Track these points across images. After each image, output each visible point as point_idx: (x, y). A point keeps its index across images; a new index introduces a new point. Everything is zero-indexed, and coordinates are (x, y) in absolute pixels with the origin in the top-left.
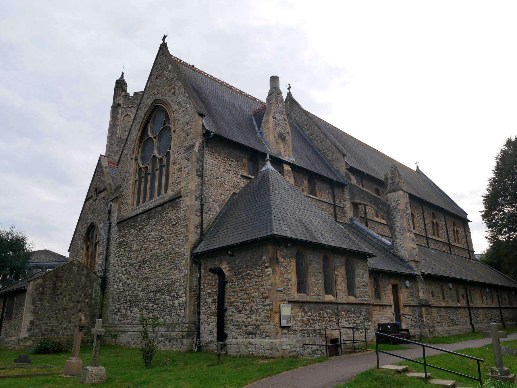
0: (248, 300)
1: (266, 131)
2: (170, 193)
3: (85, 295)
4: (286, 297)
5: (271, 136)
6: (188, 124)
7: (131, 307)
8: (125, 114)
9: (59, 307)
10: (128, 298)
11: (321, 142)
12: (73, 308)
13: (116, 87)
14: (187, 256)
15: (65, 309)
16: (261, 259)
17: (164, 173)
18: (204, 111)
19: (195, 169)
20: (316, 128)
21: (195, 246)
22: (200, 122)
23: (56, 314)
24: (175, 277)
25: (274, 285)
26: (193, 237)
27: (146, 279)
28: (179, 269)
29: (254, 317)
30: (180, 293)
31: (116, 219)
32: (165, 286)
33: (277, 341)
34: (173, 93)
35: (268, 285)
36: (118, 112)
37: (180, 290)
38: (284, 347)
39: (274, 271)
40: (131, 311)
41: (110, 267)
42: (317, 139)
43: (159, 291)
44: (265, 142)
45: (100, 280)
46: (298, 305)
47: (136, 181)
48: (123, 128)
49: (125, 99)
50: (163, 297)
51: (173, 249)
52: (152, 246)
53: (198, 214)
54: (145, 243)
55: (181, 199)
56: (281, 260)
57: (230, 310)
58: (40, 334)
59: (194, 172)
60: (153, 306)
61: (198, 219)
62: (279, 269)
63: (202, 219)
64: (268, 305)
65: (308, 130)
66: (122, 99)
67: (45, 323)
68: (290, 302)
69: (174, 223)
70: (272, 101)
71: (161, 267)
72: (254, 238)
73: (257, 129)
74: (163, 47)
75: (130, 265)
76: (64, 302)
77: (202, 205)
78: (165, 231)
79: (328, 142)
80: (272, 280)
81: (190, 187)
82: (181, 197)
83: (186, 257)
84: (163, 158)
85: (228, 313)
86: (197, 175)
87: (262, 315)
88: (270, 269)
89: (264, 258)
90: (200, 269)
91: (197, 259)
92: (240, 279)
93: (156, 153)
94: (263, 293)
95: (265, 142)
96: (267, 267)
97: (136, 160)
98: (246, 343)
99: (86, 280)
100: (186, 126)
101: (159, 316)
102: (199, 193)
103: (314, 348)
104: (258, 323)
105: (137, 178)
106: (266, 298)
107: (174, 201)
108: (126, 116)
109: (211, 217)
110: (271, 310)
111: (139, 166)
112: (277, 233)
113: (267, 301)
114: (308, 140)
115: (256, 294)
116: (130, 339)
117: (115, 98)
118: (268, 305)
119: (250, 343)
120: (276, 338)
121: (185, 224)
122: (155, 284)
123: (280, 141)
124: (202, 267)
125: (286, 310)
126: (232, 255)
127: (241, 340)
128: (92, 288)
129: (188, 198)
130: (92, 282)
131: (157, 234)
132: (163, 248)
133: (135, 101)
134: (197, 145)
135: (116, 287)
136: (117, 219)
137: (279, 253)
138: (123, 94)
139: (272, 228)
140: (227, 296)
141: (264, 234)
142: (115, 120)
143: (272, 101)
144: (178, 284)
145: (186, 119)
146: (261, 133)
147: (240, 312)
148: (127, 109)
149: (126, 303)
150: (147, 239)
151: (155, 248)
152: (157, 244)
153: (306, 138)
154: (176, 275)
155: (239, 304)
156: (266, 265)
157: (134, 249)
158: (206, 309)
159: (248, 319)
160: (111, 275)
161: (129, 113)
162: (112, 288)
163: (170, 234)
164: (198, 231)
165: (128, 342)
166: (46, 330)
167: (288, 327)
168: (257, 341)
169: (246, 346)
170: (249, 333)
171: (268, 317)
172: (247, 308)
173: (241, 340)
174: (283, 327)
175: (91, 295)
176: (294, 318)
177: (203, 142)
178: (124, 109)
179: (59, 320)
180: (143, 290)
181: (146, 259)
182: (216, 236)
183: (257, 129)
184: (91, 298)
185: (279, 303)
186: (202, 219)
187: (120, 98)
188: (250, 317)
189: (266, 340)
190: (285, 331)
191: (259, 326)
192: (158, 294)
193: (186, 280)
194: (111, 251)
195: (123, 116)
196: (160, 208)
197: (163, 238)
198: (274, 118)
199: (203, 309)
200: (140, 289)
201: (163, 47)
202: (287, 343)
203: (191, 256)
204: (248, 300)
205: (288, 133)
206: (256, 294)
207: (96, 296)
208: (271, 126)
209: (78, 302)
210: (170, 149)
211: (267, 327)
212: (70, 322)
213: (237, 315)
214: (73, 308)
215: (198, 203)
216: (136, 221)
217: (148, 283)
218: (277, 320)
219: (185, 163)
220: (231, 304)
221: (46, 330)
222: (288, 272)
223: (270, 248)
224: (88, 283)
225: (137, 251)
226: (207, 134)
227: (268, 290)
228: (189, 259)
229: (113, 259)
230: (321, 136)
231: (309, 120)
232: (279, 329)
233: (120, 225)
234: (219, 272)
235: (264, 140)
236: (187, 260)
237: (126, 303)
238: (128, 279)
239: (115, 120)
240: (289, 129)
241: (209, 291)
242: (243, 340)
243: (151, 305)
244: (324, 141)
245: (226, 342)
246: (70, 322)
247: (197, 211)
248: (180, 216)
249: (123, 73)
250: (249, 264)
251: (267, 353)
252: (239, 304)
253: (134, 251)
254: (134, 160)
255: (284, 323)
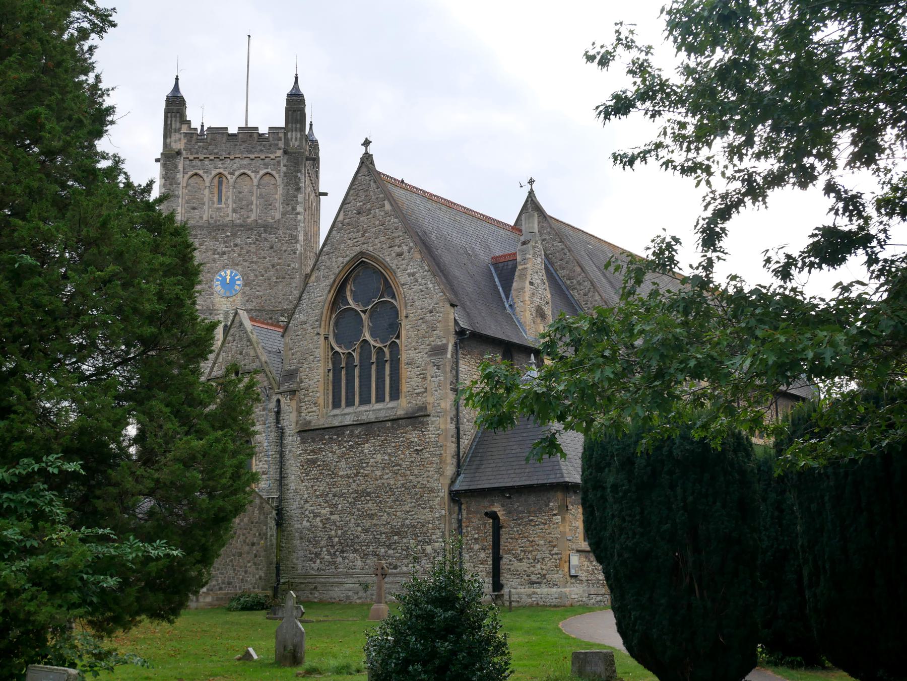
0: (531, 549)
1: (519, 305)
2: (403, 406)
3: (260, 534)
4: (574, 546)
5: (528, 314)
6: (431, 312)
7: (343, 552)
8: (190, 173)
9: (234, 551)
10: (336, 539)
11: (585, 295)
12: (248, 553)
13: (167, 112)
14: (444, 493)
15: (240, 554)
16: (547, 505)
17: (387, 372)
18: (455, 301)
19: (449, 382)
20: (578, 269)
21: (453, 482)
22: (452, 314)
23: (231, 561)
24: (423, 517)
25: (563, 534)
26: (450, 470)
27: (371, 516)
28: (431, 507)
29: (538, 566)
30: (434, 537)
31: (294, 425)
32: (409, 528)
33: (567, 590)
34: (400, 255)
35: (556, 533)
36: (176, 168)
37: (434, 534)
38: (573, 596)
39: (563, 519)
40: (344, 558)
41: (290, 494)
42: (577, 287)
43: (397, 534)
44: (519, 322)
45: (274, 512)
46: (584, 554)
47: (329, 370)
48: (187, 202)
49: (189, 141)
50: (405, 540)
51: (419, 482)
52: (378, 473)
53: (454, 440)
54: (363, 468)
55: (428, 419)
56: (570, 507)
57: (506, 559)
58: (217, 587)
59: (448, 387)
60: (386, 552)
61: (454, 446)
62: (569, 517)
63: (458, 447)
64: (556, 554)
65: (564, 268)
66: (184, 141)
67: (222, 574)
68: (578, 551)
69: (418, 448)
70: (528, 256)
71: (397, 503)
72: (540, 482)
73: (505, 300)
74: (367, 161)
75: (335, 496)
76: (239, 545)
77: (458, 429)
78: (402, 456)
79: (597, 297)
80: (561, 529)
81: (443, 405)
82: (429, 416)
83: (441, 494)
84: (386, 350)
85: (504, 561)
86: (452, 389)
87: (549, 563)
88: (559, 517)
89: (551, 504)
90: (460, 509)
91: (456, 497)
92: (520, 525)
93: (367, 336)
94: (550, 542)
95: (519, 322)
96: (555, 515)
97: (326, 338)
98: (530, 593)
99: (260, 513)
100: (429, 315)
101: (399, 564)
102: (454, 413)
103: (599, 599)
104: (544, 572)
105: (330, 367)
106: (554, 546)
107: (417, 418)
108: (192, 176)
109: (466, 442)
110: (560, 559)
111: (332, 349)
112: (567, 480)
113: (555, 550)
114: (563, 287)
115: (542, 542)
116: (350, 593)
117: (166, 136)
118: (556, 554)
119: (534, 593)
120: (566, 587)
121: (438, 452)
122: (388, 523)
123: (539, 320)
124: (463, 507)
125: (575, 560)
126: (509, 498)
127: (523, 590)
128: (266, 524)
129: (441, 420)
130: (266, 515)
131: (386, 458)
132: (400, 478)
133: (211, 148)
134: (450, 347)
135: (305, 524)
136: (297, 423)
137: (568, 500)
138: (184, 129)
139: (562, 473)
140: (502, 543)
141: (552, 480)
142: (171, 184)
143: (528, 256)
144: (431, 526)
145: (428, 303)
146: (510, 306)
147: (520, 560)
148: (194, 163)
149: (333, 546)
150: (367, 463)
151: (385, 477)
152: (387, 471)
153: (559, 281)
154: (424, 515)
155: (519, 552)
156: (555, 512)
157: (341, 473)
158: (470, 556)
159: (532, 569)
160: (293, 507)
161: (201, 172)
162: (298, 524)
163: (412, 462)
164: (455, 461)
165: (348, 597)
166: (223, 583)
167: (576, 576)
168: (543, 590)
169: (529, 596)
170: (532, 583)
171: (556, 566)
172: (530, 556)
173: (523, 590)
174: (572, 577)
175: (266, 534)
176: (580, 567)
177: (456, 343)
178: (188, 162)
179: (235, 570)
180: (366, 531)
181: (369, 490)
182: (481, 470)
183: (505, 300)
184: (266, 539)
185: (568, 552)
186: (458, 447)
187: (177, 136)
188: (534, 566)
189: (555, 590)
190: (573, 581)
191: (544, 575)
192: (396, 537)
193: (443, 521)
194: (288, 471)
195: (187, 177)
196: (389, 424)
197: (400, 465)
198: (531, 283)
199: (466, 557)
200: (359, 529)
201: (367, 161)
202: (575, 592)
203: (450, 494)
204: (531, 549)
205: (547, 303)
206: (542, 542)
207: (272, 536)
208: (527, 298)
209: (253, 544)
210: (398, 337)
211: (556, 577)
212: (246, 572)
213: (516, 564)
214: (248, 553)
215: (453, 426)
216: (343, 434)
217: (374, 522)
218: (566, 570)
219: (432, 370)
220: (509, 551)
221: (223, 583)
222: (576, 519)
223: (560, 495)
224: (262, 517)
225: (349, 477)
226: (461, 333)
227: (557, 538)
228: (446, 497)
229: (293, 482)
230: (586, 284)
231: (566, 251)
232: (569, 578)
233: (305, 434)
234: (494, 516)
235: (517, 319)
236: (443, 498)
237: (333, 546)
238: (331, 514)
239: (171, 184)
240: (549, 296)
241: (476, 536)
242: (524, 590)
243: (383, 550)
244: (590, 294)
245: (502, 592)
246: (246, 572)
247: (452, 436)
248: (428, 440)
249: (177, 79)
250: (532, 509)
251: (555, 602)
252: (519, 552)
253: (341, 477)
254: (322, 338)
255: (573, 573)
